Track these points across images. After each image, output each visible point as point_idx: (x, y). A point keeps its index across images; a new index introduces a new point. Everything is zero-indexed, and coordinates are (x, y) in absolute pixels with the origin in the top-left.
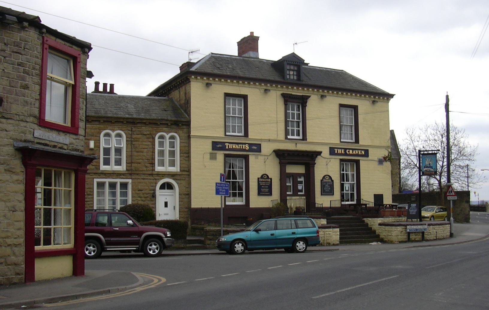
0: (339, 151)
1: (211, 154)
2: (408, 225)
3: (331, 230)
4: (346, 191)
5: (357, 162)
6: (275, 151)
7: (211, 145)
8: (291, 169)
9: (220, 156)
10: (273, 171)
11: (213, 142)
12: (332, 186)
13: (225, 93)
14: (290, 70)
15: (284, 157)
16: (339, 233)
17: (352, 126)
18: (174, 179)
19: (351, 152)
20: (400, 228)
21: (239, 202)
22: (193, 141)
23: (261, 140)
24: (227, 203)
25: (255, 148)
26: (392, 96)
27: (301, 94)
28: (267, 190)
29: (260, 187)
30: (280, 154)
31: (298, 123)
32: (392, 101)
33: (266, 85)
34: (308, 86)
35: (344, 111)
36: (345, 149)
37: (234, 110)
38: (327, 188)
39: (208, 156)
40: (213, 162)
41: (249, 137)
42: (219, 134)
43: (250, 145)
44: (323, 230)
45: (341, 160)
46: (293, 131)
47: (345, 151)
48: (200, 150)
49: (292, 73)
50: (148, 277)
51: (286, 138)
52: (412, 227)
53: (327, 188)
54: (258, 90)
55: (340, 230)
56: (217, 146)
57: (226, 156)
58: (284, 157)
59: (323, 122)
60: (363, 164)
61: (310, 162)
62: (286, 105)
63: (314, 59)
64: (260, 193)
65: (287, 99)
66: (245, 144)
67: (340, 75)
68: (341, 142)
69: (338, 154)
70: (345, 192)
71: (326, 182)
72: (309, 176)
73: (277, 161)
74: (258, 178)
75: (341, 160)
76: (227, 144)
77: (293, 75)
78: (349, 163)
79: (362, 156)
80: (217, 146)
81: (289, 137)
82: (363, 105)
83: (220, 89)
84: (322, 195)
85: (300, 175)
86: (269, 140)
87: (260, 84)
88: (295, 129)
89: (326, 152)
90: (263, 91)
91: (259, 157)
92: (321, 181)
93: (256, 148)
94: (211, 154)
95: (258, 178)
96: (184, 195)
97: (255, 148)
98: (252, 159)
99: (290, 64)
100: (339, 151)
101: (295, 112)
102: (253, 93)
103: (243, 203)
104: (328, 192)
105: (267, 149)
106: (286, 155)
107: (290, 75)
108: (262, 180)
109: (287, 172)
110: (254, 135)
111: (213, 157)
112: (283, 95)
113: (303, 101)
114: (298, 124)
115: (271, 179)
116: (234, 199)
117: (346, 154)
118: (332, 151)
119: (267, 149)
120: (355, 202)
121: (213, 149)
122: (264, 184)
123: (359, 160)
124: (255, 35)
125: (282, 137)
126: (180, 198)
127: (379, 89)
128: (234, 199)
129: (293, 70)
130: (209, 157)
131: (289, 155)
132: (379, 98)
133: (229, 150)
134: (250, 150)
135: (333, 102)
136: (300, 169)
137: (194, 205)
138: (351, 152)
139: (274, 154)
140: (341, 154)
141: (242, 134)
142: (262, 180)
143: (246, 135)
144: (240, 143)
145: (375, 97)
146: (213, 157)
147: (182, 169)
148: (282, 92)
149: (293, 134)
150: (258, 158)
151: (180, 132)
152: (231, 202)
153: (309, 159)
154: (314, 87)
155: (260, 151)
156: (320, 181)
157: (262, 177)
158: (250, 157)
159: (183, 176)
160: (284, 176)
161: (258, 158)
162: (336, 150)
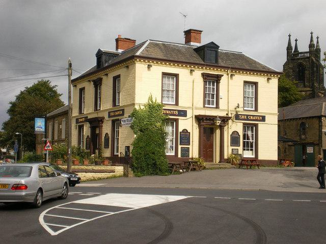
0: (243, 117)
5: (256, 125)
17: (173, 91)
19: (252, 117)
27: (217, 73)
31: (213, 95)
33: (149, 62)
35: (166, 80)
36: (247, 116)
37: (209, 88)
41: (259, 111)
43: (179, 111)
45: (244, 124)
46: (209, 101)
47: (247, 117)
51: (204, 107)
60: (261, 126)
62: (205, 82)
63: (225, 47)
67: (240, 57)
68: (244, 110)
79: (260, 121)
81: (206, 106)
83: (158, 69)
87: (144, 61)
90: (266, 79)
93: (183, 113)
98: (260, 126)
102: (261, 80)
103: (254, 156)
105: (189, 114)
112: (203, 75)
113: (217, 79)
114: (212, 98)
123: (178, 119)
125: (202, 106)
132: (236, 72)
135: (240, 78)
138: (252, 117)
141: (254, 109)
143: (177, 104)
144: (173, 110)
145: (232, 71)
148: (202, 72)
149: (209, 104)
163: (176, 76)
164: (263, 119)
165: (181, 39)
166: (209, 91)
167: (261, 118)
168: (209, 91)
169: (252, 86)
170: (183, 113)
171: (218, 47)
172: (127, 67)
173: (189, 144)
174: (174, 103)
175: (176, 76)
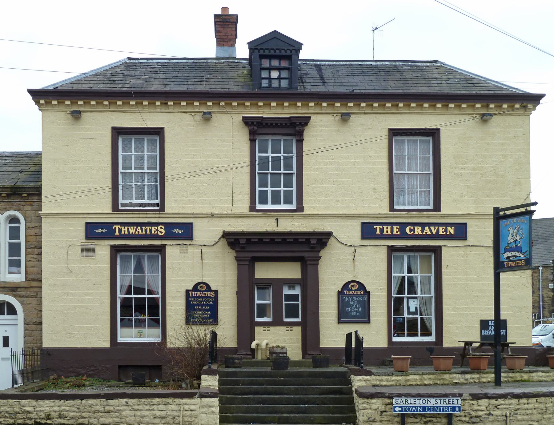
1: (83, 246)
2: (399, 396)
3: (196, 400)
4: (409, 313)
5: (437, 251)
6: (226, 235)
7: (83, 229)
8: (264, 272)
9: (103, 249)
10: (222, 275)
11: (87, 224)
12: (366, 306)
13: (113, 128)
14: (270, 69)
15: (247, 247)
16: (217, 410)
18: (15, 296)
19: (418, 230)
20: (377, 404)
21: (150, 336)
22: (46, 224)
23: (193, 215)
24: (120, 339)
25: (180, 231)
26: (536, 99)
27: (288, 116)
28: (207, 314)
29: (189, 307)
30: (233, 240)
32: (538, 115)
34: (307, 97)
36: (403, 226)
38: (354, 308)
39: (78, 251)
40: (88, 262)
41: (166, 212)
42: (100, 207)
43: (168, 226)
44: (177, 401)
45: (391, 250)
48: (61, 240)
49: (275, 74)
50: (518, 423)
51: (253, 208)
52: (433, 401)
53: (354, 308)
54: (187, 117)
55: (221, 402)
56: (95, 231)
57: (115, 250)
58: (247, 247)
59: (345, 172)
60: (451, 253)
61: (306, 255)
62: (252, 141)
64: (343, 317)
65: (256, 128)
66: (157, 224)
69: (382, 237)
70: (406, 316)
71: (351, 297)
72: (309, 283)
73: (230, 255)
74: (187, 291)
75: (391, 250)
76: (117, 227)
77: (279, 78)
78: (418, 255)
80: (95, 231)
82: (456, 129)
84: (339, 322)
85: (291, 283)
86: (212, 215)
88: (282, 189)
89: (348, 232)
90: (198, 117)
91: (190, 249)
92: (339, 293)
93: (183, 232)
94: (83, 246)
95: (187, 291)
96: (34, 324)
97: (180, 231)
98: (446, 254)
99: (271, 57)
100: (387, 230)
101: (282, 155)
102: (177, 124)
103: (159, 340)
104: (355, 317)
105: (207, 232)
106: (243, 242)
107: (270, 79)
108: (194, 294)
109: (256, 276)
110: (177, 206)
111: (87, 252)
112: (247, 121)
113: (296, 128)
115: (216, 292)
116: (140, 332)
117: (403, 236)
118: (368, 231)
119: (207, 232)
120: (431, 339)
121: (87, 237)
122: (200, 301)
123: (440, 248)
124: (231, 12)
125: (245, 207)
126: (25, 330)
127: (499, 86)
128: (140, 332)
129: (279, 69)
130: (80, 252)
131: (249, 241)
133: (122, 237)
134: (169, 236)
135: (372, 127)
136: (290, 271)
137: (50, 342)
139: (224, 242)
140: (392, 237)
142: (194, 294)
146: (87, 252)
147: (30, 277)
150: (186, 252)
151: (28, 208)
152: (128, 336)
153: (308, 248)
154: (319, 97)
155: (191, 238)
156: (336, 294)
157: (196, 288)
158: (444, 250)
159: (32, 290)
160: (247, 286)
161: (186, 252)
162: (378, 228)
163: (434, 134)
164: (461, 232)
165: (206, 47)
166: (276, 166)
167: (451, 230)
168: (276, 166)
169: (152, 143)
170: (183, 232)
171: (297, 47)
172: (76, 115)
173: (8, 314)
174: (431, 207)
175: (434, 134)
